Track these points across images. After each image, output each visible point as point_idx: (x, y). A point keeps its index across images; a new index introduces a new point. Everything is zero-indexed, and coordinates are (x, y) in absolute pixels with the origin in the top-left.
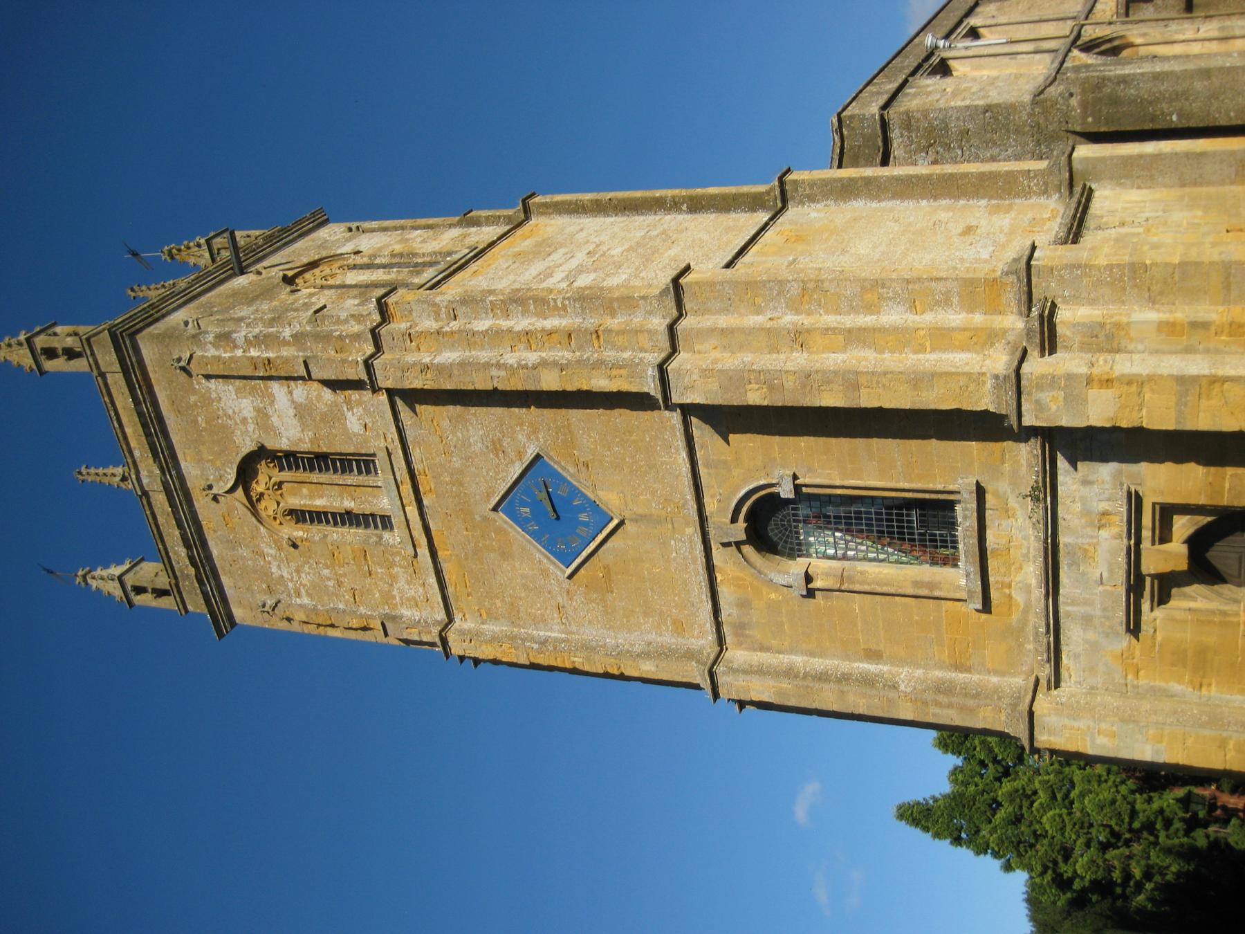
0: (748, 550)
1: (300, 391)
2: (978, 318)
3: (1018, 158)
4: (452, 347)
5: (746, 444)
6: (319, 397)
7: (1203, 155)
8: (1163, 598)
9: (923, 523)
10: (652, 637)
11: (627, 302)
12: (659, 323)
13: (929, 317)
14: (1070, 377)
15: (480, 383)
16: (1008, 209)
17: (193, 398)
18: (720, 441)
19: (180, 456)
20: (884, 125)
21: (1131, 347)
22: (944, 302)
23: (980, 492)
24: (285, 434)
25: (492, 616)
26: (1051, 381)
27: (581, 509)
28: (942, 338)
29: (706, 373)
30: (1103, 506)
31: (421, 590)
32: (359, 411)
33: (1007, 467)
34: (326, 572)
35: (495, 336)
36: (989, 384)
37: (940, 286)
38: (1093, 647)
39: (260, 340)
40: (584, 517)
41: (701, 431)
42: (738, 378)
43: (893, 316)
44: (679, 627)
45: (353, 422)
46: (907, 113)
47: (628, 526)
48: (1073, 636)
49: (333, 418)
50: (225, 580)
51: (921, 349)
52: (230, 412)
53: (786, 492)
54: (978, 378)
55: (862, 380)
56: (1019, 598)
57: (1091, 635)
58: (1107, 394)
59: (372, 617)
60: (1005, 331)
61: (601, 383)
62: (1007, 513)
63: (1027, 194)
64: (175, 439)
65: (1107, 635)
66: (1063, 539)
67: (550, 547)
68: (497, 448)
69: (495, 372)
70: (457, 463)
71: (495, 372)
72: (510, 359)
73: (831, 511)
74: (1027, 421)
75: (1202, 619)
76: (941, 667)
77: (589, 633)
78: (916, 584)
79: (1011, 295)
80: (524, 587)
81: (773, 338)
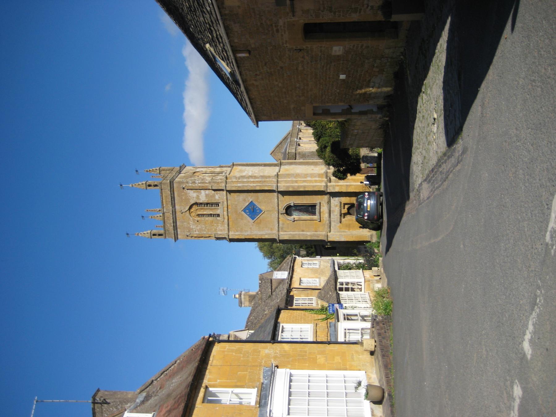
0: (285, 215)
1: (207, 192)
2: (320, 179)
3: (316, 160)
4: (240, 184)
5: (286, 197)
6: (211, 193)
8: (344, 217)
9: (311, 209)
10: (267, 232)
11: (269, 177)
12: (275, 180)
13: (313, 179)
14: (333, 185)
15: (246, 189)
16: (317, 167)
17: (183, 194)
18: (282, 197)
19: (176, 205)
20: (296, 154)
22: (315, 177)
23: (320, 203)
25: (237, 231)
26: (331, 186)
27: (258, 210)
28: (316, 181)
29: (284, 186)
30: (337, 204)
32: (218, 195)
33: (324, 199)
34: (203, 226)
35: (248, 182)
36: (323, 187)
37: (315, 175)
38: (335, 225)
39: (201, 183)
40: (258, 211)
41: (280, 196)
42: (288, 187)
43: (309, 179)
44: (272, 229)
45: (217, 197)
46: (299, 152)
47: (266, 212)
48: (333, 224)
49: (214, 196)
50: (178, 230)
51: (313, 183)
53: (292, 205)
54: (321, 186)
56: (325, 219)
57: (335, 224)
58: (338, 187)
59: (212, 234)
61: (266, 188)
62: (324, 206)
63: (319, 165)
64: (176, 201)
66: (331, 209)
67: (251, 217)
68: (244, 200)
69: (248, 187)
70: (236, 203)
71: (248, 187)
72: (251, 185)
73: (298, 208)
74: (328, 191)
75: (349, 220)
76: (313, 232)
77: (255, 232)
78: (310, 218)
79: (324, 176)
80: (245, 225)
81: (293, 182)
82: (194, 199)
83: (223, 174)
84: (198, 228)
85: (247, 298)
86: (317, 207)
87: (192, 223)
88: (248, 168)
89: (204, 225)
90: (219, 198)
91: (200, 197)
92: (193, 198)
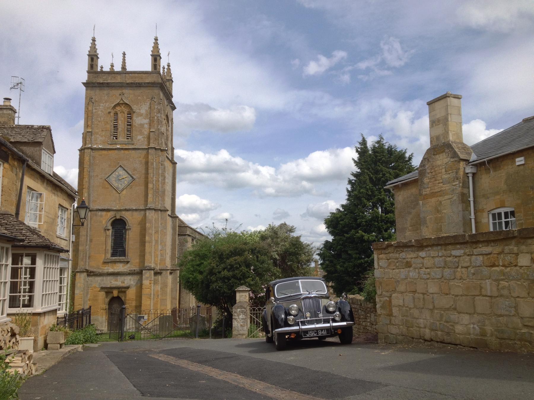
7: (177, 292)
17: (145, 97)
20: (185, 235)
21: (155, 286)
24: (137, 119)
30: (126, 282)
31: (99, 143)
34: (102, 119)
45: (140, 137)
49: (141, 133)
52: (142, 107)
55: (151, 244)
56: (106, 268)
58: (148, 283)
60: (157, 266)
65: (100, 284)
90: (139, 140)
91: (140, 118)
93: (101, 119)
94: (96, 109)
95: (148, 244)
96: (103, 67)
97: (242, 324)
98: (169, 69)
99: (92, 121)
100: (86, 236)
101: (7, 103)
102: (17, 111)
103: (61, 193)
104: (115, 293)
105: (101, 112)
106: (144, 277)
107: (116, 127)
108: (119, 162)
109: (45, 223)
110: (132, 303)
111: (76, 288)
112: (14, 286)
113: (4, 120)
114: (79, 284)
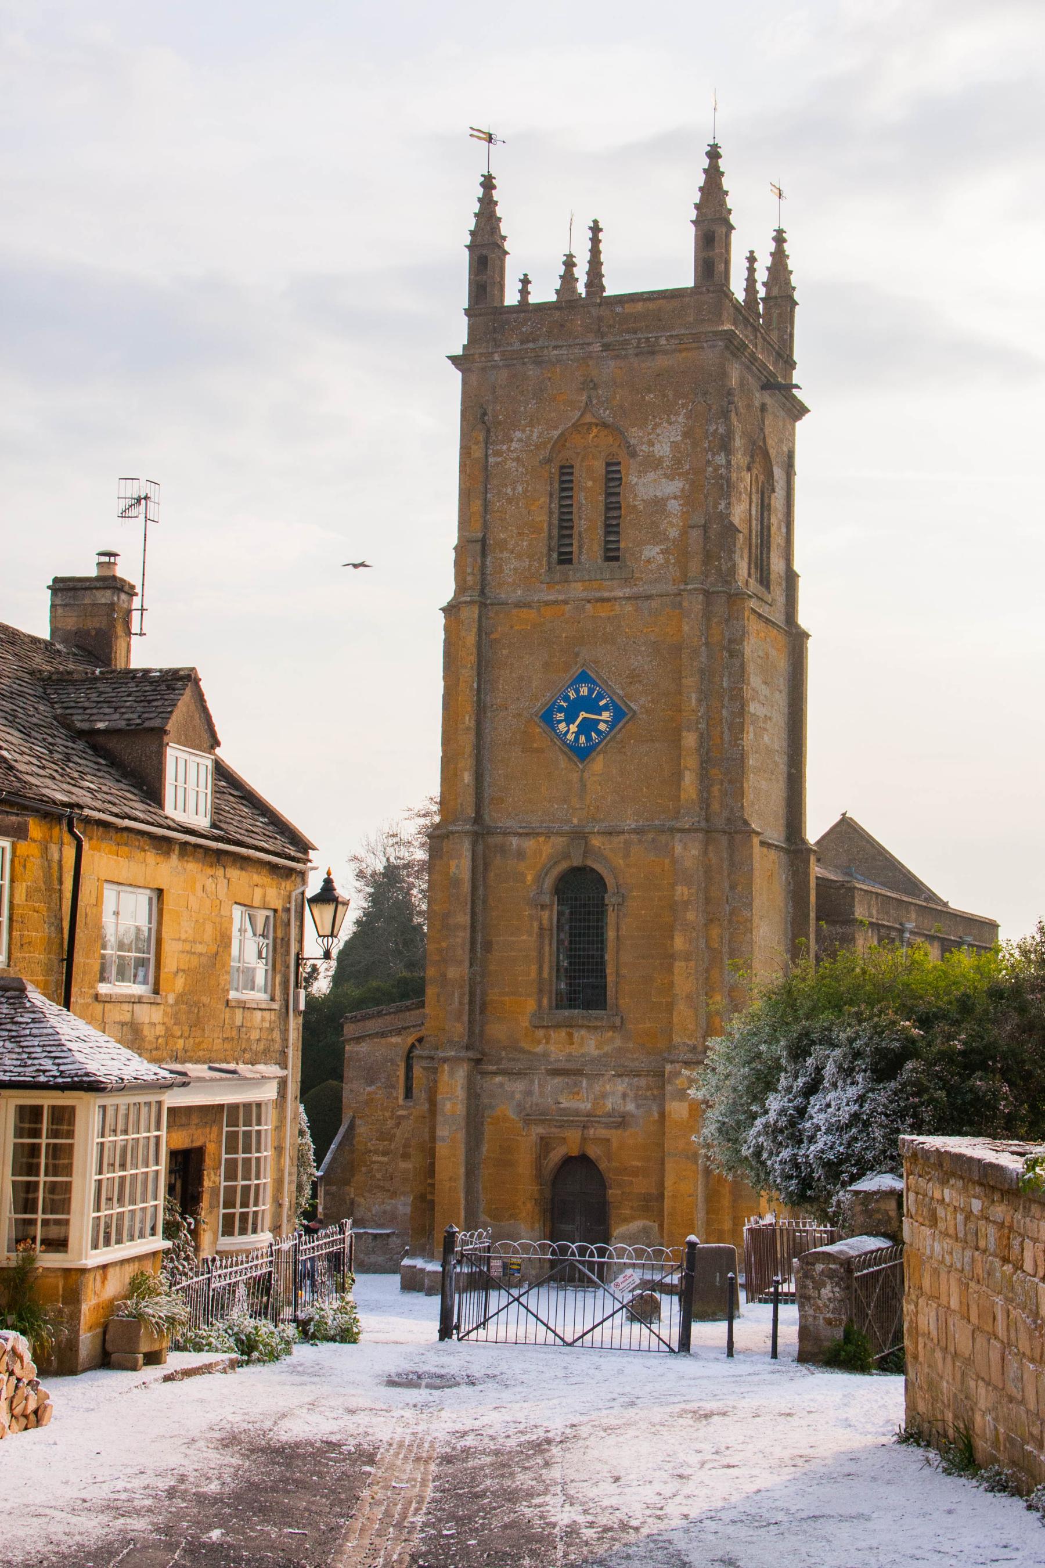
17: (670, 394)
34: (520, 489)
45: (652, 551)
49: (657, 536)
52: (658, 431)
82: (644, 448)
83: (754, 586)
84: (511, 465)
85: (93, 624)
86: (554, 1004)
87: (535, 435)
88: (781, 699)
89: (525, 491)
90: (649, 561)
91: (651, 476)
92: (651, 444)
93: (514, 489)
94: (498, 453)
95: (683, 964)
96: (530, 278)
97: (830, 1315)
98: (779, 256)
99: (485, 499)
100: (468, 931)
101: (108, 573)
102: (138, 590)
103: (242, 869)
104: (571, 1143)
105: (514, 464)
106: (669, 1088)
107: (565, 526)
108: (577, 649)
109: (181, 974)
110: (631, 1183)
111: (440, 1119)
112: (471, 1002)
113: (98, 625)
114: (448, 1106)
